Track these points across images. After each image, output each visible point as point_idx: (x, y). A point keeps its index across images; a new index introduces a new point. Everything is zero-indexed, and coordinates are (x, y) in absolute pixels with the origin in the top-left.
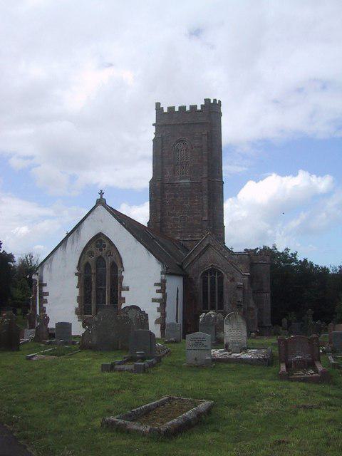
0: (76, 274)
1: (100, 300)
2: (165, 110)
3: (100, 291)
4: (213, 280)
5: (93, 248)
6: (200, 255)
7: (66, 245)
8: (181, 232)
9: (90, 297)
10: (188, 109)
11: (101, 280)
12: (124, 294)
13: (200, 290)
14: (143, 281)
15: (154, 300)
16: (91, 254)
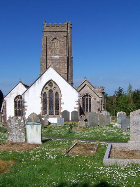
0: (40, 97)
1: (51, 108)
7: (35, 84)
9: (46, 107)
11: (51, 100)
12: (62, 106)
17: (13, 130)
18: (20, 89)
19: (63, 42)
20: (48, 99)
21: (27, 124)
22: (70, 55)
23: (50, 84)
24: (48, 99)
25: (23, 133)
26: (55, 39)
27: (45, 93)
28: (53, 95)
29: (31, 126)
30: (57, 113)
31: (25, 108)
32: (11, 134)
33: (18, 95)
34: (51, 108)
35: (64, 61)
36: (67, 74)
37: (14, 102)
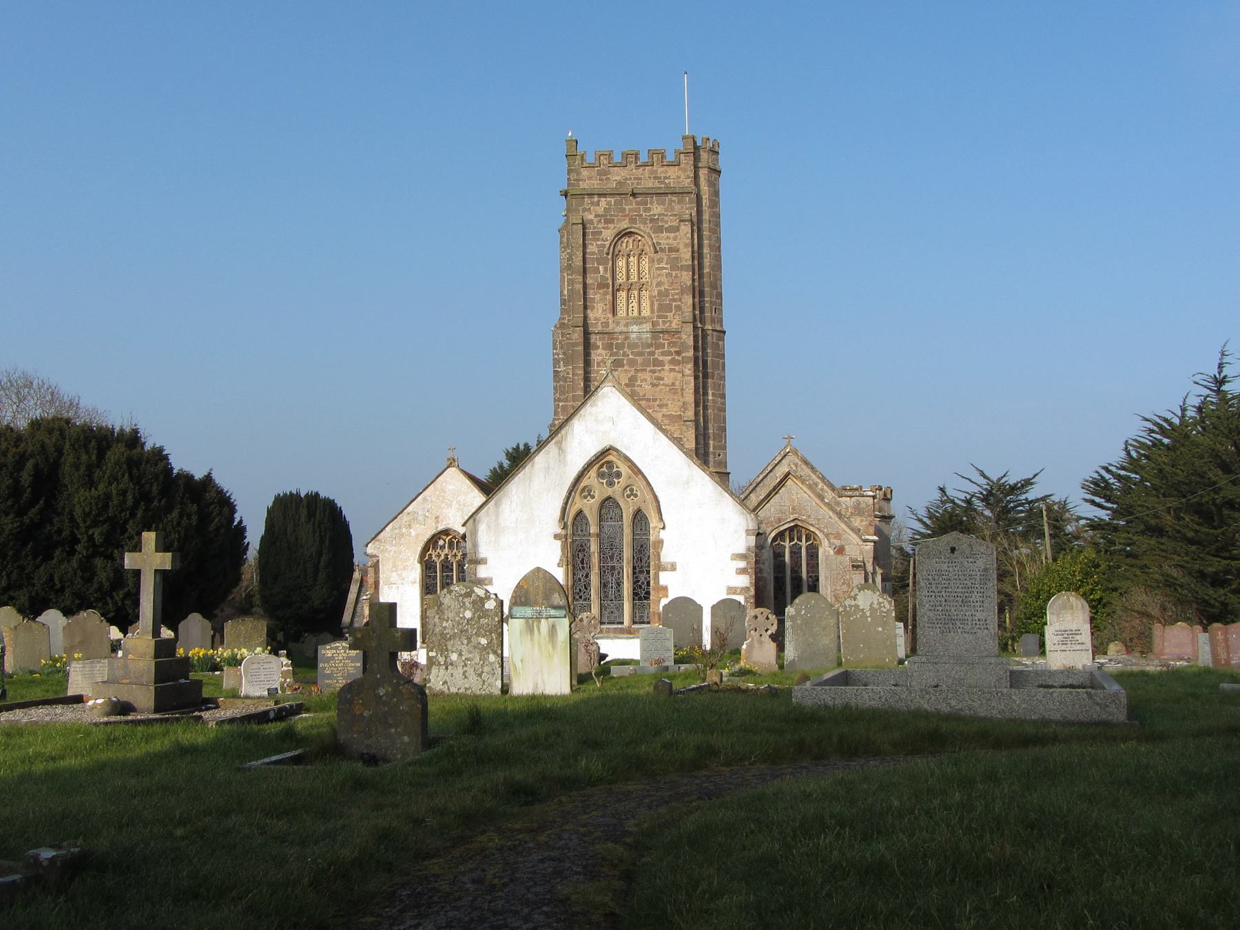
0: (556, 537)
1: (610, 592)
3: (609, 571)
4: (795, 553)
5: (591, 479)
6: (768, 497)
9: (587, 586)
11: (610, 551)
12: (665, 578)
17: (450, 644)
18: (452, 499)
20: (594, 547)
21: (511, 616)
22: (713, 321)
23: (604, 469)
24: (594, 547)
25: (495, 653)
27: (580, 512)
28: (621, 527)
29: (527, 623)
30: (640, 618)
32: (442, 660)
33: (441, 528)
34: (610, 592)
35: (678, 353)
36: (692, 424)
37: (419, 565)
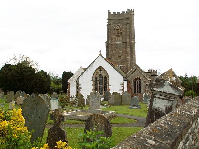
2: (112, 13)
3: (101, 86)
4: (137, 82)
7: (87, 71)
8: (119, 63)
10: (121, 13)
12: (109, 87)
13: (133, 86)
14: (116, 83)
15: (120, 90)
16: (97, 73)
19: (126, 28)
20: (98, 83)
24: (98, 83)
26: (119, 26)
31: (80, 89)
